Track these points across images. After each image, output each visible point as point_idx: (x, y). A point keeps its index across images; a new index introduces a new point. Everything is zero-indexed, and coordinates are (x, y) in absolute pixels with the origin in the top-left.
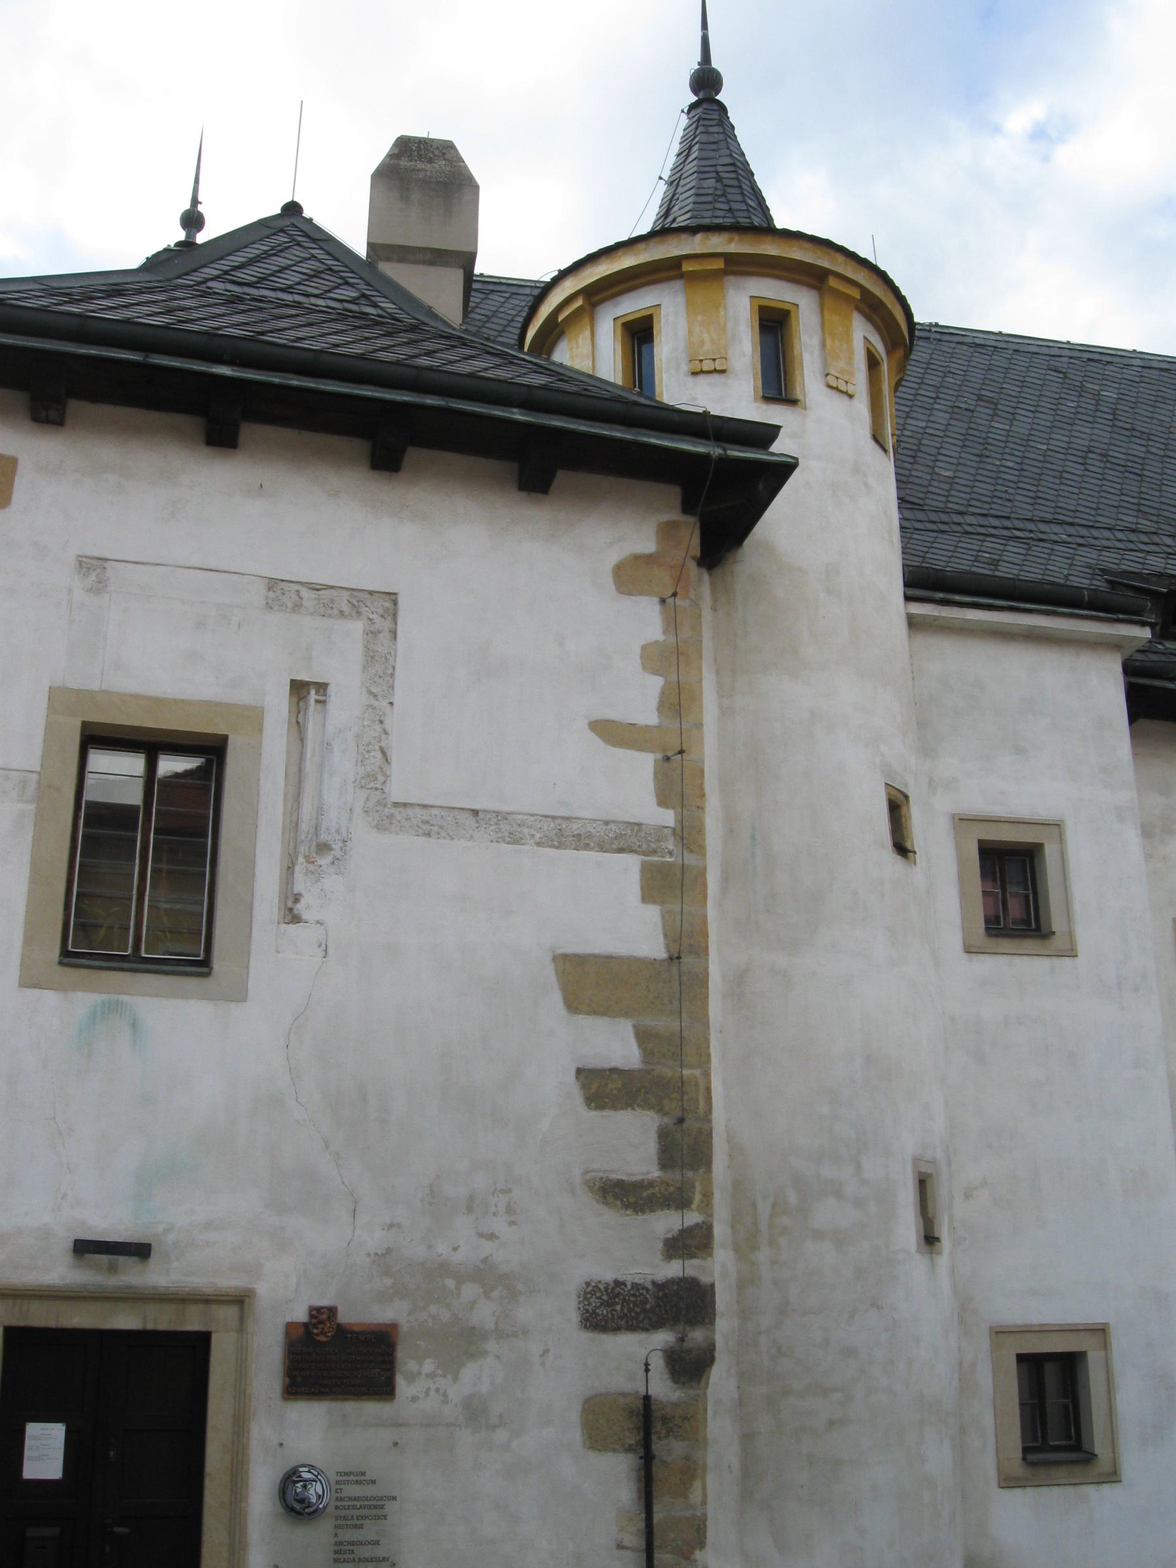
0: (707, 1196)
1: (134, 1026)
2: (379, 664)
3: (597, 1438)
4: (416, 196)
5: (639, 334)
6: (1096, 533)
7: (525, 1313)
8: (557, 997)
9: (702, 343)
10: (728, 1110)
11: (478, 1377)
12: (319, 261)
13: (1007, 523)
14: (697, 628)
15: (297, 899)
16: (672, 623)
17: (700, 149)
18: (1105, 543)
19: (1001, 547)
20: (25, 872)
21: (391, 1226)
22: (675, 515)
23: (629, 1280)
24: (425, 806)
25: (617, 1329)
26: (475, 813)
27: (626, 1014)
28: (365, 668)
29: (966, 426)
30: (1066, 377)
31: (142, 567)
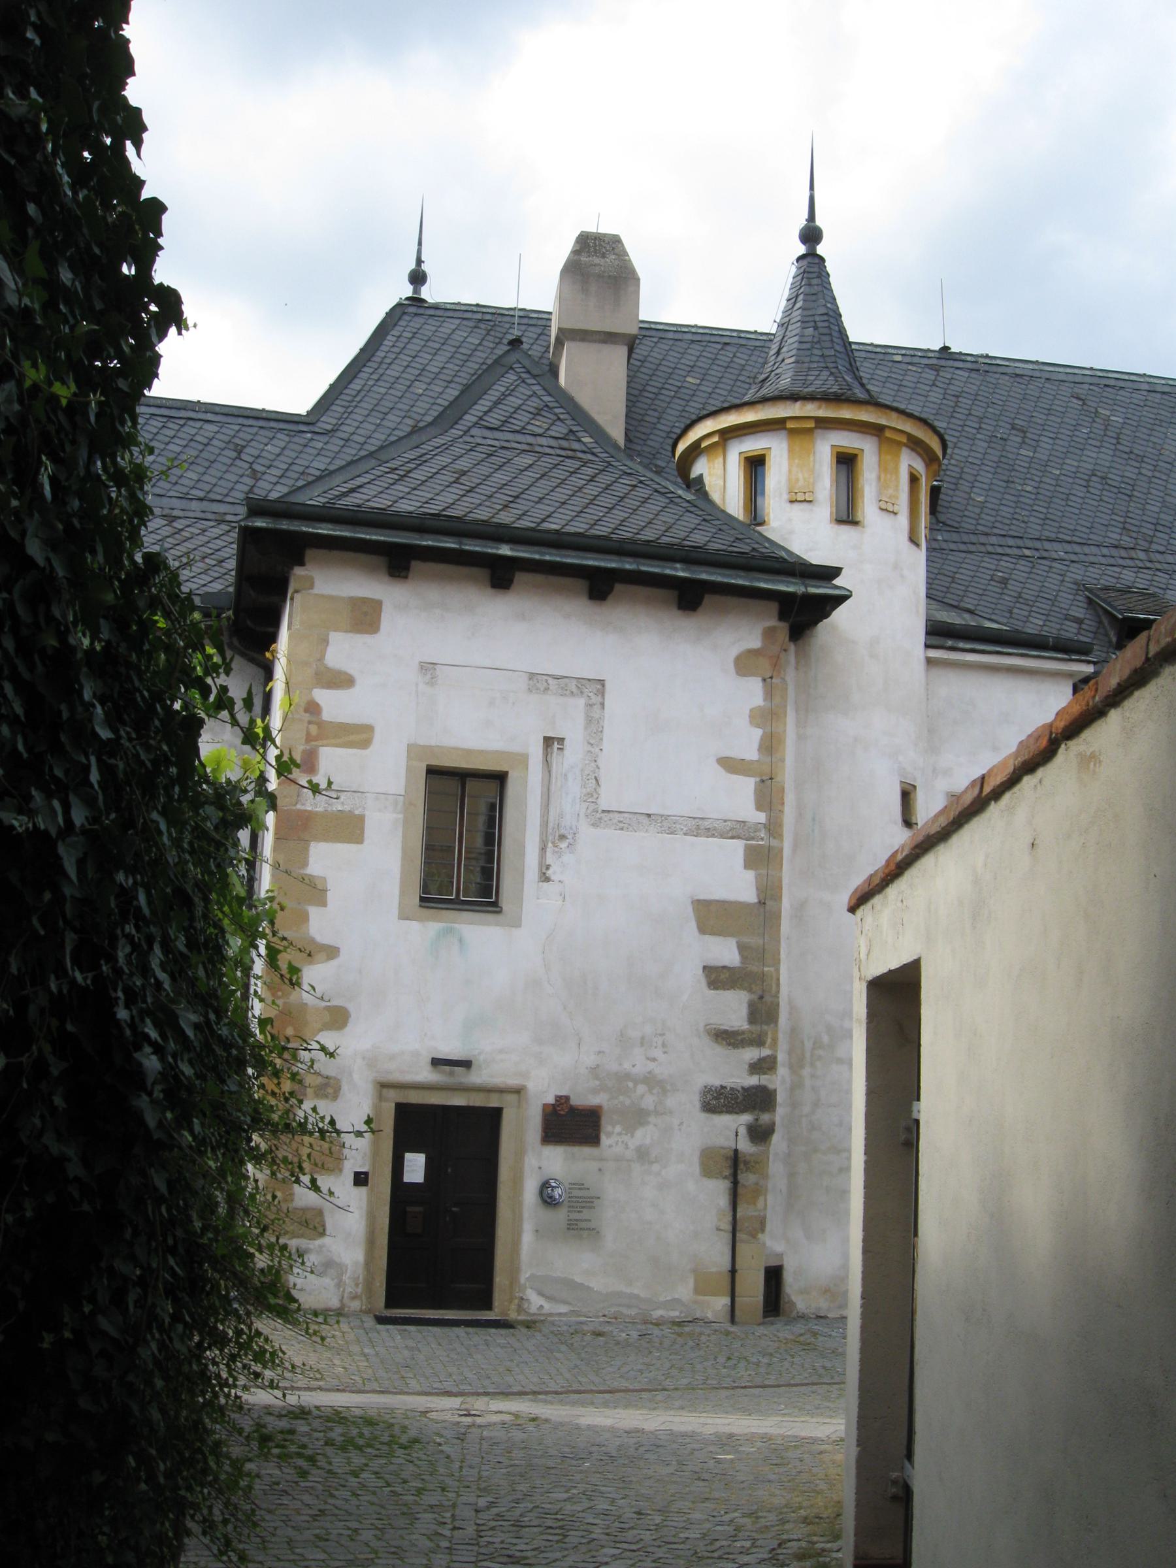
0: (775, 1041)
1: (460, 940)
2: (594, 726)
3: (707, 1171)
5: (755, 465)
6: (1086, 549)
8: (693, 925)
9: (797, 480)
10: (790, 986)
11: (644, 1136)
13: (1019, 542)
14: (784, 697)
15: (548, 867)
16: (769, 693)
17: (804, 300)
18: (1092, 559)
19: (1012, 566)
20: (399, 853)
21: (600, 1052)
22: (773, 622)
23: (729, 1085)
24: (620, 812)
25: (721, 1112)
26: (649, 815)
27: (732, 935)
28: (586, 728)
29: (999, 453)
30: (1084, 404)
31: (909, 1349)
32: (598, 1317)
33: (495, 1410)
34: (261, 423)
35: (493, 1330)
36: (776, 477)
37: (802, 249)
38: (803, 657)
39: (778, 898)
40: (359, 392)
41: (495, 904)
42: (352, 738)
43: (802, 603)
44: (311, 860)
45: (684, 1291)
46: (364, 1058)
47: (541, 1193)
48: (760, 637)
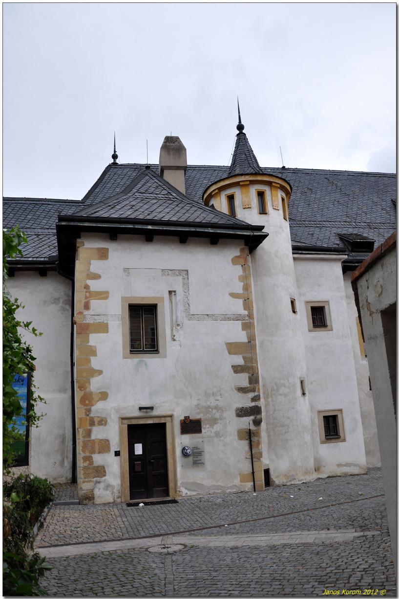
0: (259, 389)
1: (146, 364)
2: (186, 285)
3: (240, 438)
4: (171, 153)
5: (231, 198)
6: (336, 223)
7: (225, 415)
8: (226, 351)
11: (217, 427)
12: (157, 183)
13: (315, 223)
14: (249, 271)
15: (174, 336)
16: (244, 270)
18: (339, 226)
22: (243, 246)
24: (198, 315)
25: (243, 416)
26: (208, 315)
27: (240, 354)
28: (183, 287)
32: (207, 495)
33: (176, 543)
34: (67, 204)
35: (170, 505)
36: (238, 202)
37: (238, 132)
38: (254, 260)
39: (254, 340)
40: (98, 192)
41: (157, 350)
42: (101, 296)
43: (251, 240)
44: (90, 340)
45: (237, 481)
46: (115, 410)
47: (183, 452)
48: (239, 252)
